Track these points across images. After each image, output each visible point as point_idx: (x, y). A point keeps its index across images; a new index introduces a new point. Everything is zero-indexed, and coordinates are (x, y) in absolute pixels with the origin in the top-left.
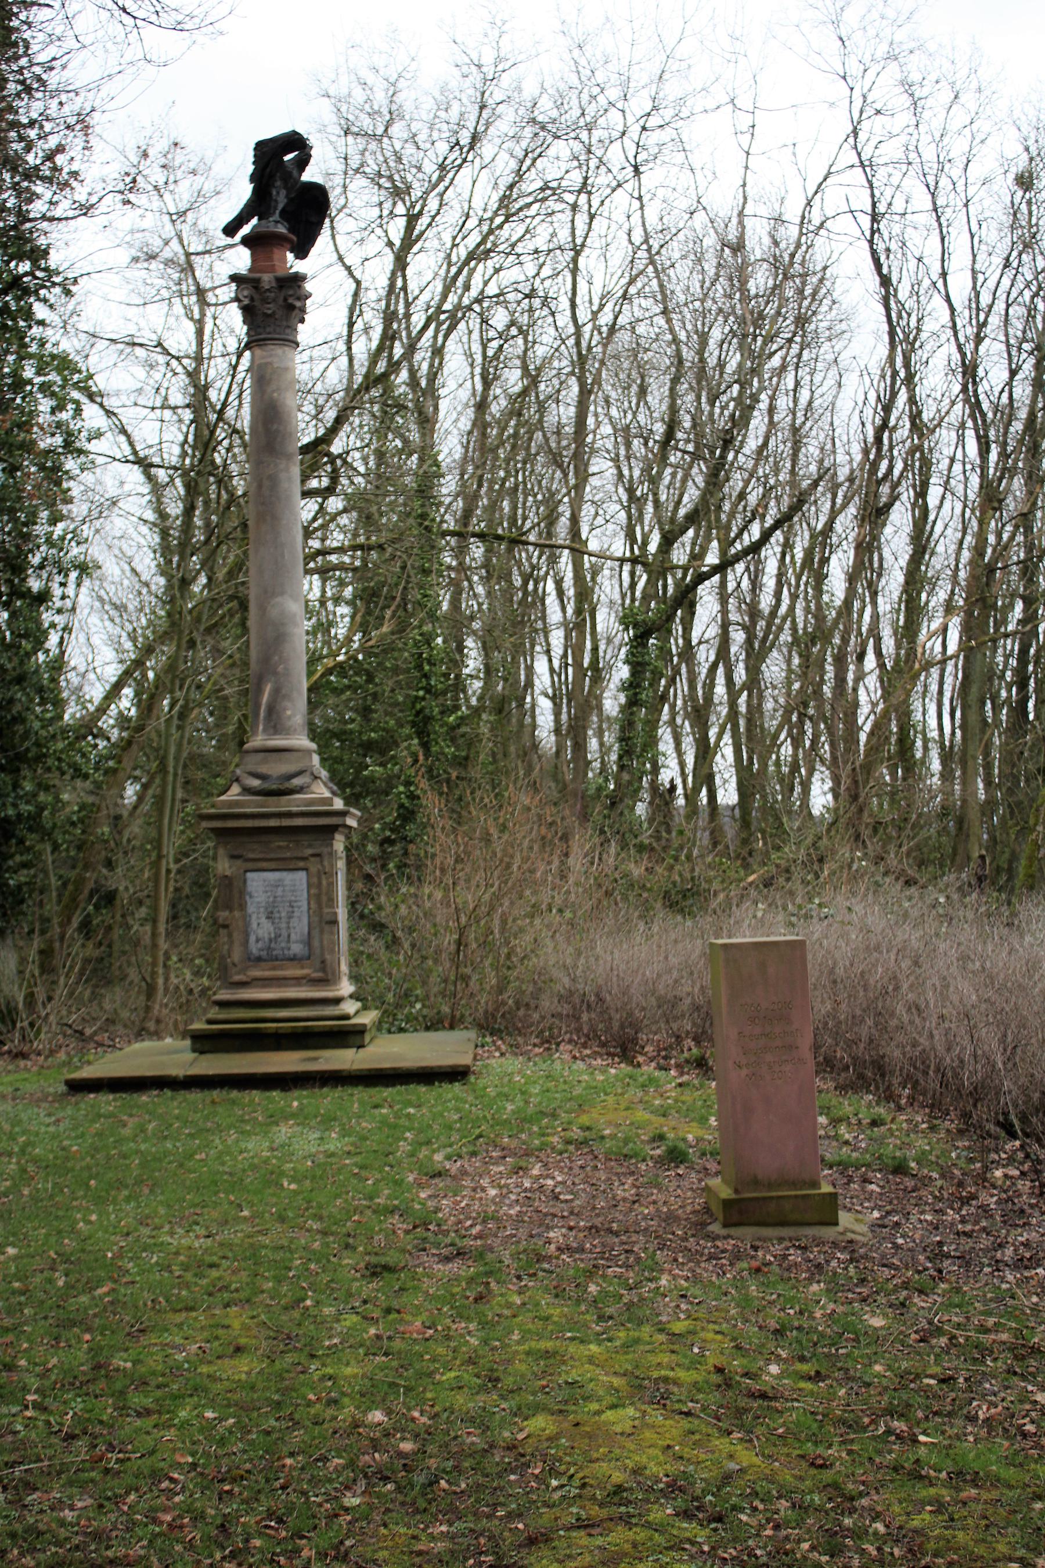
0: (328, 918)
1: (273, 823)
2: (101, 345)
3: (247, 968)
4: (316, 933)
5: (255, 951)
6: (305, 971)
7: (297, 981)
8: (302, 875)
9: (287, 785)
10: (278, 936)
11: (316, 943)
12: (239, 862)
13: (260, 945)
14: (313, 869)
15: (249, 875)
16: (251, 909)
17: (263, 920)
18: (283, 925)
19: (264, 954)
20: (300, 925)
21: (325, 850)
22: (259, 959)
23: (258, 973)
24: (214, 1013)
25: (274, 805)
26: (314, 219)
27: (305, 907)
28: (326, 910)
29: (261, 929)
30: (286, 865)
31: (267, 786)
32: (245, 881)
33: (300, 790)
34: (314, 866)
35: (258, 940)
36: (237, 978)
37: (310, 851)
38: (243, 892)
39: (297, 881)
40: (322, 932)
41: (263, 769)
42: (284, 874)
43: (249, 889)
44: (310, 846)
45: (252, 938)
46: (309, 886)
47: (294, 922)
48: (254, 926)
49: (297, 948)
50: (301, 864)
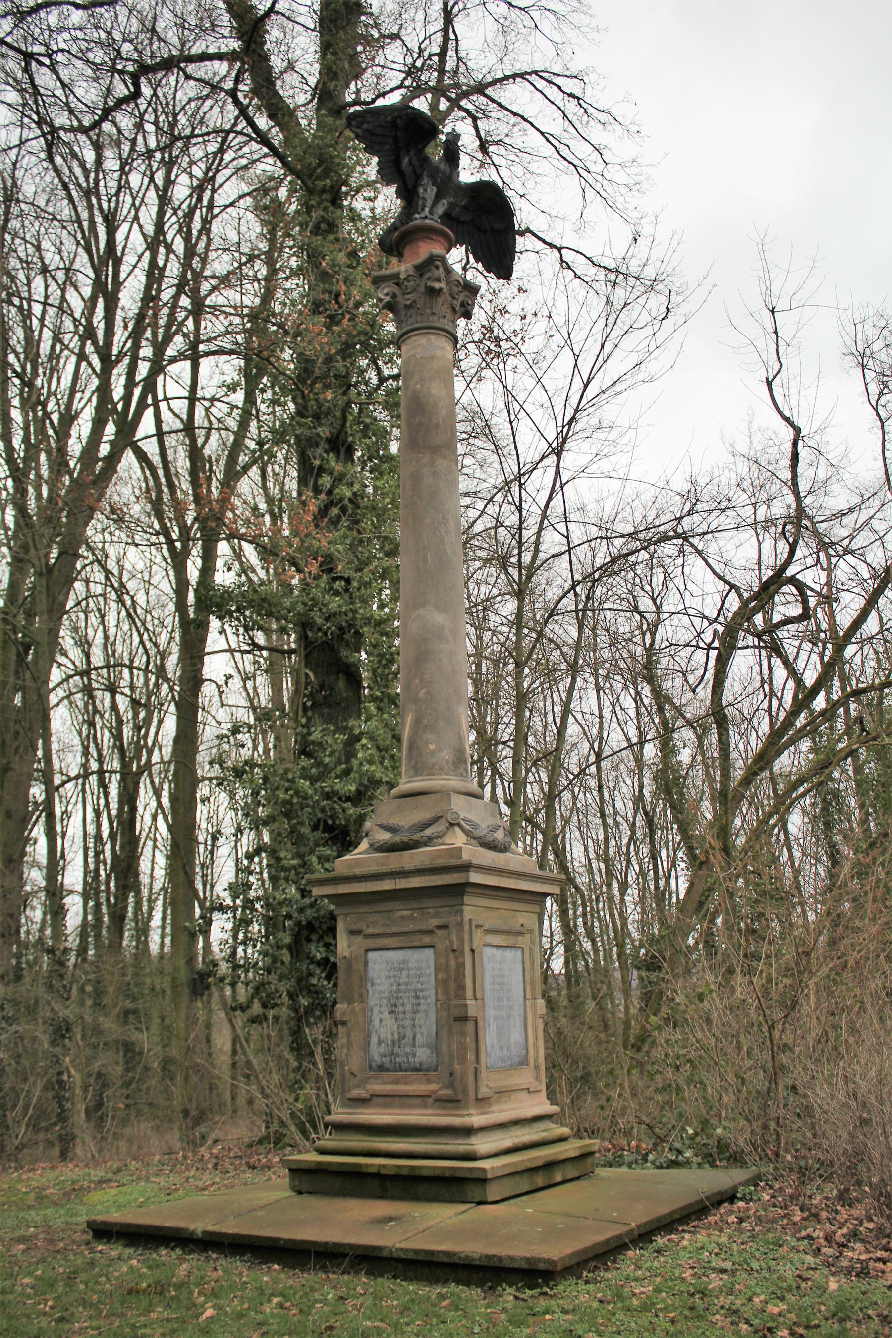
0: (456, 1012)
1: (387, 885)
2: (823, 575)
3: (365, 1081)
4: (444, 1034)
5: (376, 1057)
6: (433, 1087)
7: (422, 1099)
8: (429, 953)
9: (417, 837)
10: (402, 1037)
11: (444, 1049)
12: (358, 939)
13: (382, 1049)
14: (440, 946)
15: (371, 955)
16: (373, 1001)
17: (386, 1015)
18: (408, 1023)
19: (386, 1060)
20: (427, 1023)
21: (452, 920)
22: (381, 1068)
23: (377, 1087)
24: (329, 1141)
25: (396, 861)
26: (499, 226)
27: (432, 999)
28: (455, 1002)
29: (384, 1027)
30: (411, 941)
31: (398, 839)
32: (366, 964)
33: (429, 841)
34: (441, 940)
35: (380, 1042)
36: (356, 1093)
37: (435, 922)
38: (364, 978)
39: (424, 960)
40: (450, 1032)
41: (394, 821)
42: (409, 953)
43: (371, 974)
44: (437, 915)
45: (374, 1039)
46: (437, 969)
47: (420, 1019)
48: (376, 1023)
49: (423, 1055)
50: (427, 939)
